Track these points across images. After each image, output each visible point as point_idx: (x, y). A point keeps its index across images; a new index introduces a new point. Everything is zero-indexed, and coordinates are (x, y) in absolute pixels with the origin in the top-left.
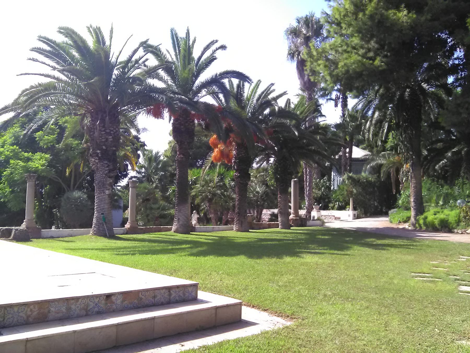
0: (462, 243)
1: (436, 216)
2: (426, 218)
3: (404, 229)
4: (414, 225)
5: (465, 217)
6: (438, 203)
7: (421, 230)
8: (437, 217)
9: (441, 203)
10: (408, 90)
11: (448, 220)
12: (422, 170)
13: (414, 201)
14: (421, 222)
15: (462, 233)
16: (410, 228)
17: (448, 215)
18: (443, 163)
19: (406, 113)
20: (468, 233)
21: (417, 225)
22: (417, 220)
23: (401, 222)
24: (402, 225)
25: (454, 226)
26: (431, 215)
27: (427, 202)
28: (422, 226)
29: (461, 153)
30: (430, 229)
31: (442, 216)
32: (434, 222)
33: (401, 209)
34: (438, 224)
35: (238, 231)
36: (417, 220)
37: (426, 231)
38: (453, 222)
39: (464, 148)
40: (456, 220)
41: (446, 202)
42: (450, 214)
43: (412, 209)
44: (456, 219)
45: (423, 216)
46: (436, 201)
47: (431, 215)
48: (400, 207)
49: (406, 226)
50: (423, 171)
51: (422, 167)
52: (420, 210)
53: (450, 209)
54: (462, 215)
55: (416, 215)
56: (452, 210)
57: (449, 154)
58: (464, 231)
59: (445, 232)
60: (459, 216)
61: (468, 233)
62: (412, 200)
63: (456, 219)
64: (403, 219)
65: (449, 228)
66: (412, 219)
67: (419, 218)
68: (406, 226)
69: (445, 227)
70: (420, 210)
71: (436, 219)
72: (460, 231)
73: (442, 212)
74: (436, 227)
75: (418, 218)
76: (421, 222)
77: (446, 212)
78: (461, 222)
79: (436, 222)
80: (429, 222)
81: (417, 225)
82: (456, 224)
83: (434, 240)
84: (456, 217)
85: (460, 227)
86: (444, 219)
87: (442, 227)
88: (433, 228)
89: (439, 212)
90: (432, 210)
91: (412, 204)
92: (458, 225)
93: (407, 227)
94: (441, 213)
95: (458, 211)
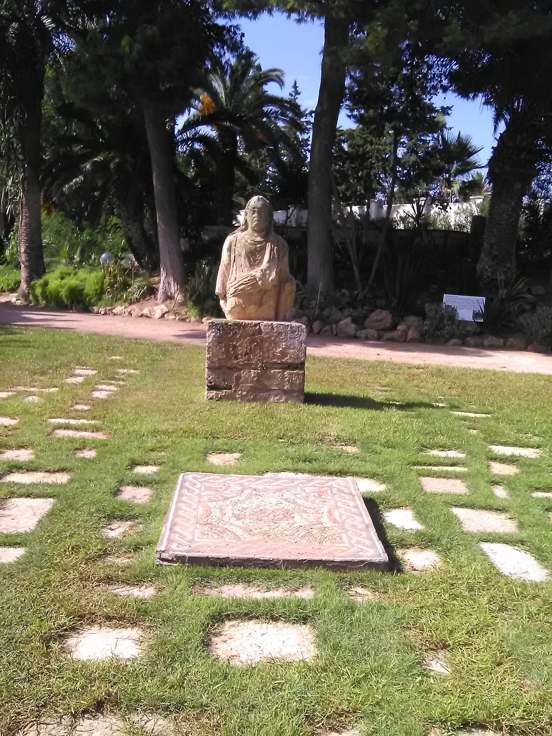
0: (96, 334)
1: (64, 281)
2: (46, 284)
3: (8, 303)
4: (25, 296)
5: (111, 285)
6: (72, 259)
7: (37, 308)
8: (66, 284)
9: (77, 258)
10: (15, 25)
11: (83, 290)
12: (42, 193)
13: (25, 252)
14: (38, 291)
15: (105, 314)
16: (18, 303)
17: (84, 281)
18: (76, 183)
19: (12, 74)
20: (115, 314)
21: (31, 297)
22: (32, 288)
23: (4, 291)
24: (6, 296)
25: (93, 301)
26: (54, 281)
27: (52, 256)
28: (40, 298)
29: (109, 165)
30: (53, 304)
31: (72, 281)
32: (59, 292)
33: (9, 266)
34: (66, 296)
35: (159, 275)
36: (32, 288)
37: (46, 308)
38: (91, 293)
39: (114, 158)
40: (96, 290)
41: (84, 257)
42: (88, 279)
43: (23, 266)
44: (97, 287)
45: (41, 281)
46: (69, 255)
47: (54, 281)
48: (8, 264)
49: (13, 298)
50: (45, 195)
51: (41, 186)
52: (37, 269)
53: (88, 268)
54: (107, 280)
55: (29, 279)
56: (92, 271)
57: (88, 166)
58: (109, 310)
59: (78, 312)
60: (103, 283)
61: (115, 314)
62: (23, 250)
63: (97, 287)
64: (8, 285)
65: (84, 305)
66: (24, 286)
67: (34, 285)
68: (13, 298)
69: (78, 302)
70: (37, 269)
71: (62, 287)
72: (102, 310)
73: (75, 274)
74: (62, 302)
75: (32, 283)
76: (38, 291)
77: (82, 274)
78: (104, 293)
79: (63, 293)
80: (50, 293)
81: (31, 297)
82: (96, 298)
83: (50, 328)
84: (98, 283)
85: (102, 303)
86: (76, 287)
87: (72, 302)
88: (57, 303)
89: (69, 274)
90: (61, 269)
91: (23, 257)
92: (100, 299)
93: (14, 300)
94: (72, 276)
95: (101, 274)
